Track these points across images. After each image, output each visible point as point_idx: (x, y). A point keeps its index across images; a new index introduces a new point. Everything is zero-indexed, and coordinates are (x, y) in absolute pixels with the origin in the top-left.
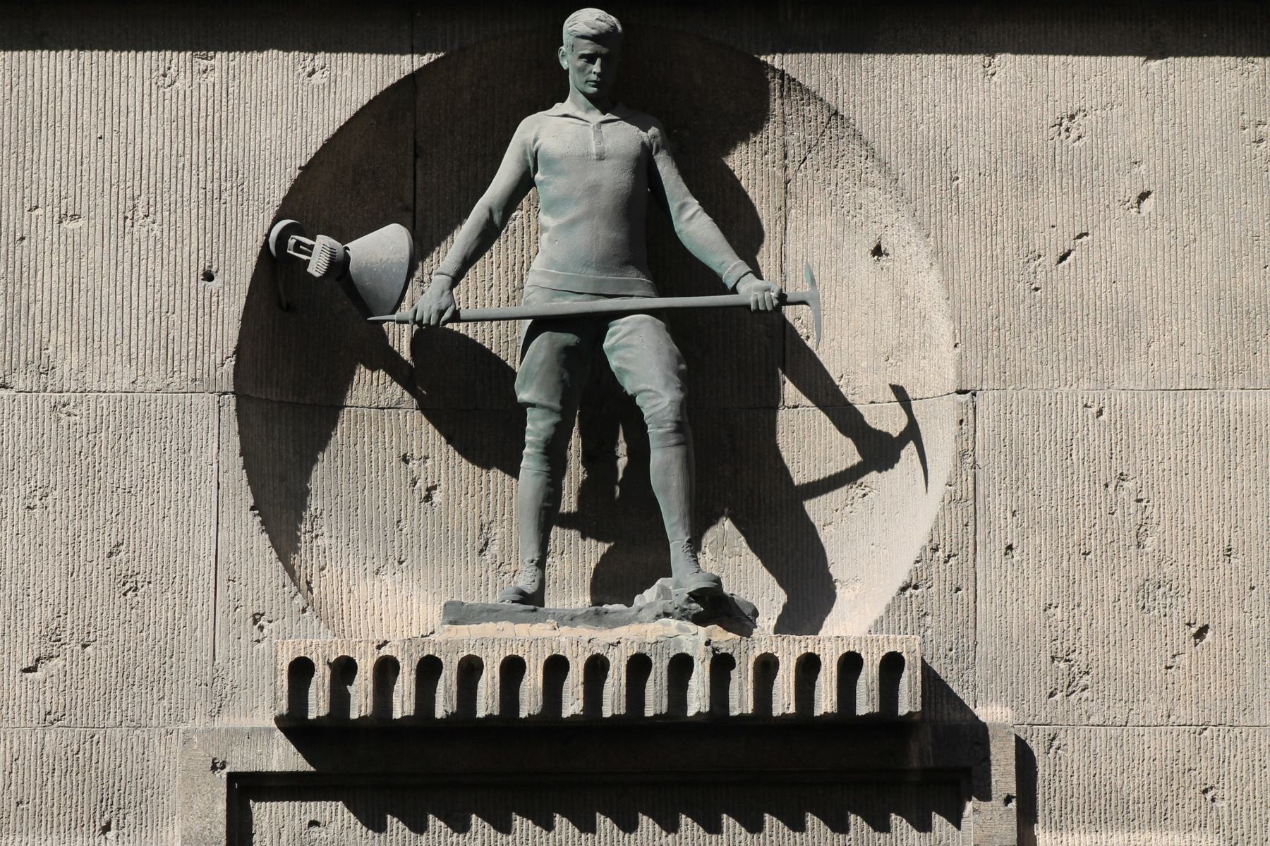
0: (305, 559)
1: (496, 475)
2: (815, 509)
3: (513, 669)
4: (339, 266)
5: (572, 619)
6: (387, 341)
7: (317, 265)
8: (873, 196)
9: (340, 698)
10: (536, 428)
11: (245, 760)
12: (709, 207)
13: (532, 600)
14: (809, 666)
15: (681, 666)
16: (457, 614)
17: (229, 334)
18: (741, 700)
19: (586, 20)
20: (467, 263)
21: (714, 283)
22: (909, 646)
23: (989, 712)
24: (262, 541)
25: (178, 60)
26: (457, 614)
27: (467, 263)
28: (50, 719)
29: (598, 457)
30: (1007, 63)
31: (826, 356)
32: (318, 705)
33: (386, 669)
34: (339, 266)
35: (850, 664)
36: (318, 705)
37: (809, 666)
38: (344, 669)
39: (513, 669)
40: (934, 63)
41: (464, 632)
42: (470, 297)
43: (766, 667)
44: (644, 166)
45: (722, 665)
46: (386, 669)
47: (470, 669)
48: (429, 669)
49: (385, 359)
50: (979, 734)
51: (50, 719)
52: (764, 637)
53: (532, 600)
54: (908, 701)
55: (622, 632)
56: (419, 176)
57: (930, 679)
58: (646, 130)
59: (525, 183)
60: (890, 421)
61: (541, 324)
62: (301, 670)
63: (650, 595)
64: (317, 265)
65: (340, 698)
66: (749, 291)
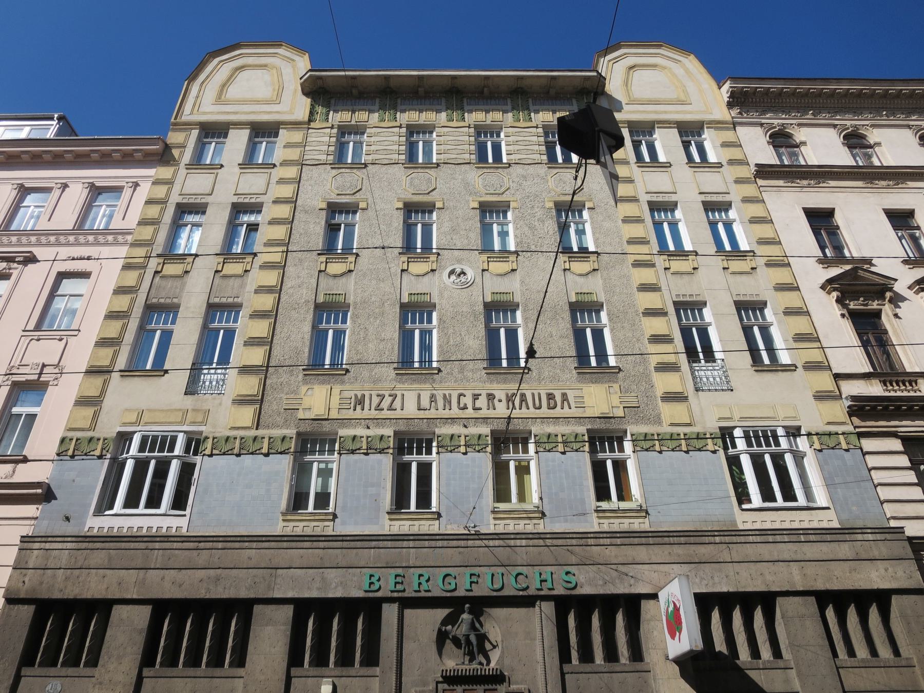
0: (442, 659)
1: (53, 501)
2: (489, 653)
3: (462, 670)
4: (445, 629)
5: (467, 665)
6: (58, 128)
7: (443, 630)
8: (493, 622)
9: (446, 673)
10: (463, 646)
11: (437, 680)
12: (479, 623)
13: (463, 663)
14: (489, 669)
15: (477, 670)
16: (457, 665)
17: (435, 636)
18: (483, 673)
19: (467, 606)
20: (457, 629)
21: (479, 631)
22: (497, 667)
23: (506, 674)
24: (439, 657)
25: (430, 610)
26: (457, 665)
27: (457, 629)
28: (419, 676)
29: (469, 648)
30: (505, 609)
31: (490, 638)
32: (444, 674)
33: (450, 670)
34: (445, 629)
35: (493, 669)
36: (444, 674)
37: (489, 669)
38: (447, 671)
39: (462, 670)
40: (498, 609)
41: (458, 667)
42: (457, 633)
43: (485, 670)
44: (473, 620)
45: (481, 670)
46: (450, 670)
47: (458, 670)
48: (454, 670)
49: (449, 638)
50: (505, 676)
51: (419, 676)
52: (485, 667)
53: (463, 663)
54: (498, 673)
55: (472, 666)
56: (333, 183)
57: (501, 671)
58: (449, 686)
59: (462, 621)
60: (495, 644)
61: (464, 635)
62: (443, 671)
63: (474, 662)
64: (443, 630)
65: (446, 673)
66: (483, 632)
